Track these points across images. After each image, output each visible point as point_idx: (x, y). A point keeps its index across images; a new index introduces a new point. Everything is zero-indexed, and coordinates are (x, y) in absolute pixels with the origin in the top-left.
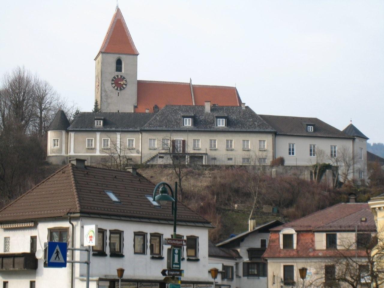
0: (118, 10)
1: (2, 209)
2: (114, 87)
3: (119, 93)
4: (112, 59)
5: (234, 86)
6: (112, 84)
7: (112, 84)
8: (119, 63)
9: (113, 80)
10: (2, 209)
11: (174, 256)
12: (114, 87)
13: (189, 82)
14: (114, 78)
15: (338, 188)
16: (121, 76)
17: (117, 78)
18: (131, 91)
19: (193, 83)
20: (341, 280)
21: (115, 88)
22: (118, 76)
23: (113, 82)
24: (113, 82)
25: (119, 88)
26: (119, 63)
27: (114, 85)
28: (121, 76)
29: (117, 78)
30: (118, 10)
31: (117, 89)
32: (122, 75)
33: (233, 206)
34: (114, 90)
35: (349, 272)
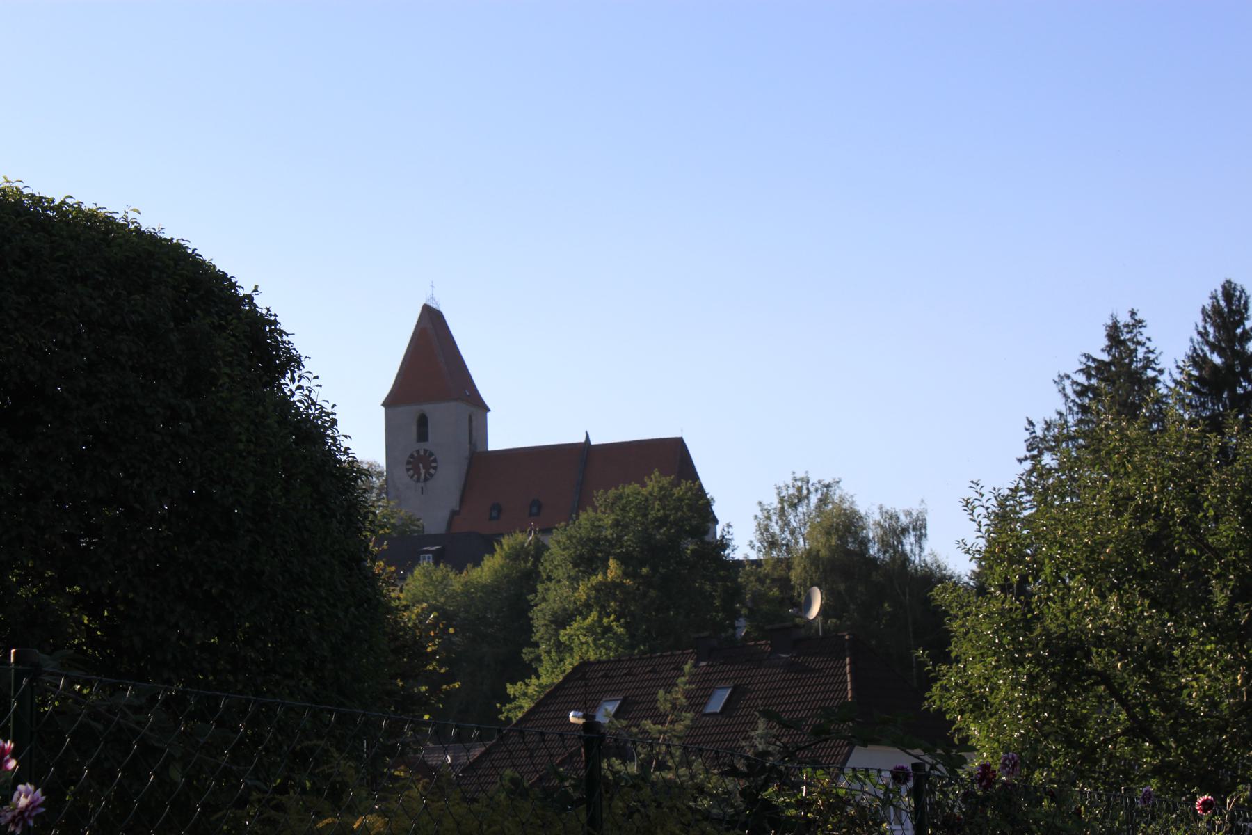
2: (412, 477)
4: (409, 413)
5: (679, 436)
6: (408, 470)
7: (408, 470)
8: (423, 422)
9: (408, 462)
11: (428, 535)
12: (412, 477)
13: (582, 439)
14: (412, 456)
15: (1032, 633)
17: (432, 458)
18: (449, 478)
20: (578, 561)
23: (410, 466)
24: (410, 466)
26: (423, 422)
28: (426, 451)
29: (432, 458)
32: (426, 448)
33: (100, 222)
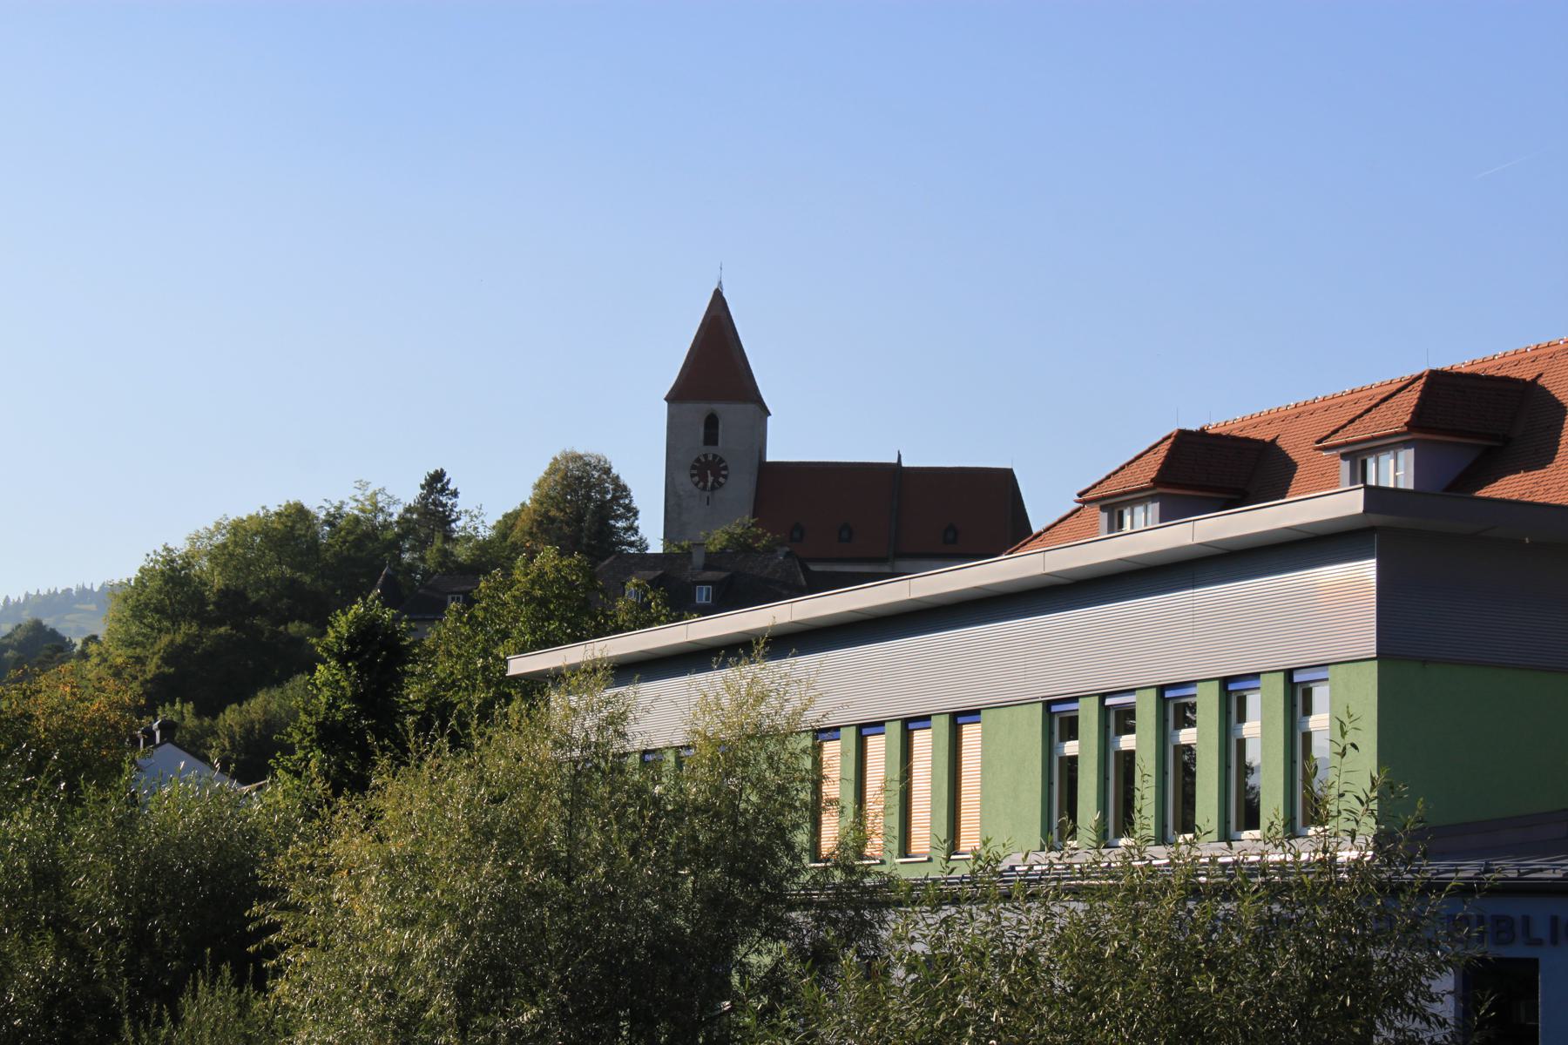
0: (718, 301)
1: (1019, 545)
2: (696, 485)
3: (708, 498)
4: (696, 412)
7: (692, 476)
8: (712, 423)
9: (693, 467)
10: (1019, 545)
13: (895, 461)
14: (698, 460)
16: (715, 456)
18: (741, 486)
19: (905, 464)
21: (699, 486)
22: (706, 456)
23: (695, 472)
24: (695, 472)
25: (723, 472)
26: (712, 423)
27: (696, 479)
28: (715, 456)
30: (718, 301)
31: (725, 468)
34: (697, 491)
35: (1411, 1028)
